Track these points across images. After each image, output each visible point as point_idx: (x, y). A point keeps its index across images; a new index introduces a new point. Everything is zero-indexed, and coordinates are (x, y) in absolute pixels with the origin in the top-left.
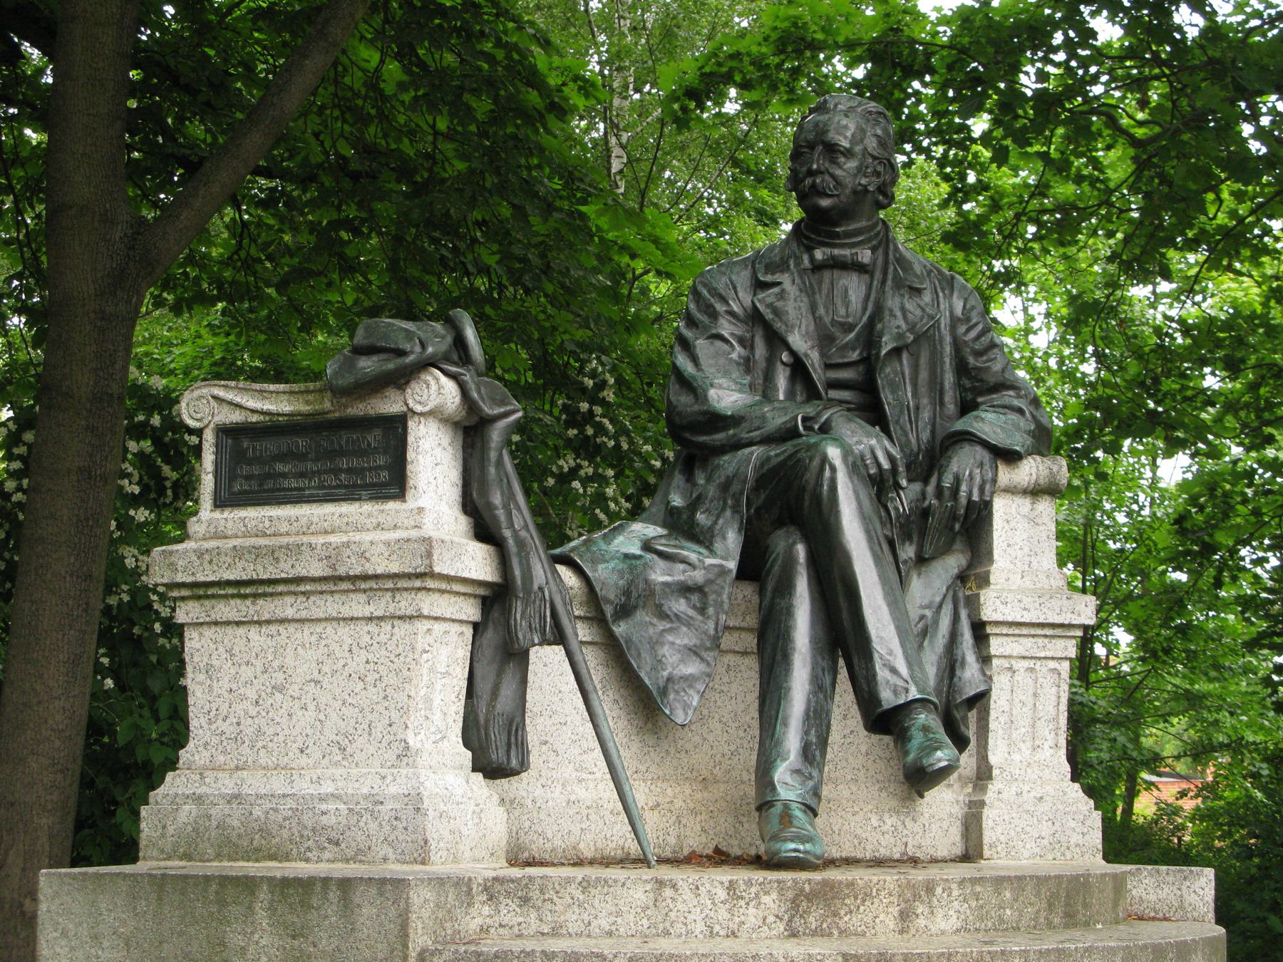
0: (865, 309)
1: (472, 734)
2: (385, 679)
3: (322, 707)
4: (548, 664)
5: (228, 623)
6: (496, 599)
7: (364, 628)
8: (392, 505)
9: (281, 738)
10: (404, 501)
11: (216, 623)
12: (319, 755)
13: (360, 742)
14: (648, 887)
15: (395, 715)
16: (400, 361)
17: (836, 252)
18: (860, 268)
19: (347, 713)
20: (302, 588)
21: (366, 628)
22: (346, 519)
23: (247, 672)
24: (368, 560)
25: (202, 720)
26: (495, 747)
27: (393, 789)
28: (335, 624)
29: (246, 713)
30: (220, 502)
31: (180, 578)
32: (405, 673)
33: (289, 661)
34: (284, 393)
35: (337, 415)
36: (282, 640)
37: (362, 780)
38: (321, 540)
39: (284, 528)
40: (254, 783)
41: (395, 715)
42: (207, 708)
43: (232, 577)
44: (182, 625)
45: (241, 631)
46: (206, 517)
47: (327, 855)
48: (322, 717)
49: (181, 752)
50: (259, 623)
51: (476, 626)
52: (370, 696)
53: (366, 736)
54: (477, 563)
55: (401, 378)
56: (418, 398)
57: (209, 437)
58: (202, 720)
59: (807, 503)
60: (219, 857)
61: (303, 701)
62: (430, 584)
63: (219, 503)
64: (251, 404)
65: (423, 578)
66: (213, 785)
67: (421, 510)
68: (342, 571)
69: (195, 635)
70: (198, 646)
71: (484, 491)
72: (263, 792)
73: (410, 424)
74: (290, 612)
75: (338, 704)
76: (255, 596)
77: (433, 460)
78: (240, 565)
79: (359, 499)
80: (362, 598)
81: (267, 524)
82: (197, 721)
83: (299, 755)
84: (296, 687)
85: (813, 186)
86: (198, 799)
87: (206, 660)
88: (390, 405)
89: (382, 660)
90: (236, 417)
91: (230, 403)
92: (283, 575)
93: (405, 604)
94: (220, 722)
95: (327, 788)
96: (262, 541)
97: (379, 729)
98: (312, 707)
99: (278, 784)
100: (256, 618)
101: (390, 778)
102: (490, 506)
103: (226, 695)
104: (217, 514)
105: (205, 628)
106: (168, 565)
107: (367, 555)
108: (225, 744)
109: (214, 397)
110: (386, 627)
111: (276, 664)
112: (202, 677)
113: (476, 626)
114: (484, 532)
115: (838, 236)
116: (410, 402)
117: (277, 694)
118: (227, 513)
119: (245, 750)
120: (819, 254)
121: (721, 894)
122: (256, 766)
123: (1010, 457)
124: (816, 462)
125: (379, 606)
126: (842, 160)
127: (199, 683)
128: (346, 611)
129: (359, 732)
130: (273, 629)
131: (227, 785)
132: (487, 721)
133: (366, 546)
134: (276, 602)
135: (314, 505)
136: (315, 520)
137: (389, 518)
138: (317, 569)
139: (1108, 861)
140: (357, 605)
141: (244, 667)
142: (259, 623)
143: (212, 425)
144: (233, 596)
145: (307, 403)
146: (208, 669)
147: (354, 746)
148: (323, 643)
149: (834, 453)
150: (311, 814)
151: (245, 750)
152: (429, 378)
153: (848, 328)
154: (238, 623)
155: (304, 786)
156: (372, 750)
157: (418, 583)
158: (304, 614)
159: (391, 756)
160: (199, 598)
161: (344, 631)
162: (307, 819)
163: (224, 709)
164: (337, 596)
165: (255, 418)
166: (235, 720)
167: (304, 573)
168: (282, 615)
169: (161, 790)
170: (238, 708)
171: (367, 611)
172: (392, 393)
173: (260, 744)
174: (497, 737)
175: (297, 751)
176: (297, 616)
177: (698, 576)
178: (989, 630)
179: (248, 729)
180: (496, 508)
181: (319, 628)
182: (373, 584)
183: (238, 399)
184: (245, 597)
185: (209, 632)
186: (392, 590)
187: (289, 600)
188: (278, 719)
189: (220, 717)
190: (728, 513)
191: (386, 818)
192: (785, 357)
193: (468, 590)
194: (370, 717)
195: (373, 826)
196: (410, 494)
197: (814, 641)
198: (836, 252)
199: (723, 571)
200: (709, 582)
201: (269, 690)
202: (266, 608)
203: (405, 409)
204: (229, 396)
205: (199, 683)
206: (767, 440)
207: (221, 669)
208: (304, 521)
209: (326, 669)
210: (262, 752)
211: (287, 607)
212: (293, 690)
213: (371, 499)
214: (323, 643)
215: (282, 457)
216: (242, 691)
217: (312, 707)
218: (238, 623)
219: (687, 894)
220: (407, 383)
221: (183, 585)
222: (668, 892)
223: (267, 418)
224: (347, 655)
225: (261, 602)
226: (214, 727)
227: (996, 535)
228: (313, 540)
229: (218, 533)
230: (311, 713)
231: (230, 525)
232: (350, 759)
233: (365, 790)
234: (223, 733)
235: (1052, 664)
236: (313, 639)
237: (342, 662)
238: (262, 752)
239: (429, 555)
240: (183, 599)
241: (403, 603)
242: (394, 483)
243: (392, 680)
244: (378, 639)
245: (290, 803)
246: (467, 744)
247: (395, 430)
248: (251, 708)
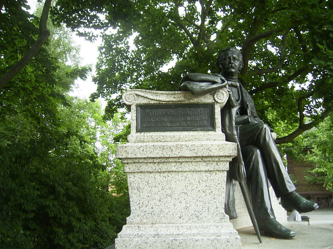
0: (239, 96)
2: (214, 192)
3: (188, 202)
7: (204, 174)
9: (171, 213)
10: (215, 131)
12: (188, 219)
13: (204, 214)
17: (233, 83)
18: (236, 87)
19: (198, 204)
20: (180, 160)
21: (205, 175)
22: (194, 137)
23: (155, 190)
24: (211, 151)
25: (136, 207)
28: (192, 173)
29: (155, 204)
30: (137, 131)
31: (129, 156)
33: (173, 185)
34: (165, 94)
35: (187, 102)
37: (209, 227)
39: (169, 139)
42: (138, 202)
45: (152, 175)
48: (188, 205)
49: (127, 218)
52: (208, 198)
53: (207, 211)
55: (212, 92)
56: (219, 98)
57: (133, 108)
58: (136, 207)
61: (180, 200)
63: (137, 131)
64: (151, 97)
66: (144, 230)
69: (132, 176)
70: (134, 180)
72: (168, 233)
73: (215, 106)
74: (174, 169)
78: (156, 152)
79: (197, 130)
80: (204, 164)
81: (162, 138)
83: (179, 219)
84: (176, 195)
85: (232, 66)
87: (137, 185)
89: (212, 185)
90: (145, 101)
91: (143, 97)
92: (175, 156)
94: (144, 207)
95: (195, 231)
97: (212, 209)
100: (159, 171)
101: (220, 227)
103: (147, 198)
104: (139, 134)
105: (136, 174)
107: (210, 149)
108: (146, 215)
109: (137, 95)
111: (167, 187)
112: (136, 191)
115: (233, 79)
116: (216, 99)
117: (169, 198)
118: (142, 134)
126: (236, 61)
127: (134, 193)
128: (198, 169)
129: (204, 211)
130: (166, 174)
134: (168, 165)
136: (182, 137)
137: (212, 137)
141: (154, 188)
142: (160, 172)
143: (135, 104)
145: (174, 98)
147: (202, 215)
148: (188, 179)
150: (191, 241)
151: (155, 217)
156: (210, 217)
158: (180, 169)
161: (196, 175)
163: (146, 203)
164: (193, 163)
165: (153, 102)
166: (151, 207)
168: (171, 170)
169: (120, 233)
170: (152, 203)
172: (208, 96)
173: (162, 215)
175: (178, 218)
176: (177, 170)
179: (157, 210)
181: (185, 174)
182: (210, 159)
183: (146, 95)
185: (137, 175)
186: (217, 161)
187: (173, 164)
188: (169, 206)
189: (144, 206)
191: (224, 242)
194: (208, 205)
198: (233, 83)
201: (165, 196)
202: (164, 167)
203: (213, 101)
205: (134, 193)
208: (177, 137)
209: (189, 188)
210: (163, 218)
213: (201, 130)
214: (188, 179)
216: (153, 196)
217: (184, 202)
223: (158, 102)
224: (198, 184)
225: (161, 165)
226: (141, 209)
228: (187, 143)
231: (146, 138)
232: (201, 220)
234: (145, 211)
236: (183, 178)
237: (196, 186)
238: (163, 218)
241: (221, 166)
244: (210, 178)
248: (157, 202)
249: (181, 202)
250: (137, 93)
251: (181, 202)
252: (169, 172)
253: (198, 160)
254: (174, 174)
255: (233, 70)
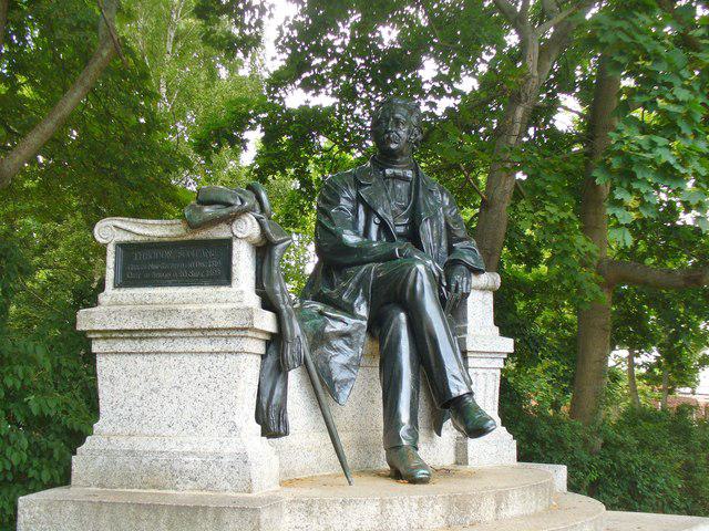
1: (261, 416)
4: (294, 377)
5: (124, 353)
6: (276, 341)
7: (207, 358)
8: (223, 289)
11: (116, 353)
14: (378, 504)
15: (227, 408)
16: (230, 209)
17: (396, 171)
18: (405, 179)
23: (135, 381)
26: (271, 421)
27: (228, 450)
30: (117, 286)
31: (96, 328)
32: (233, 384)
33: (161, 375)
36: (157, 363)
38: (183, 308)
39: (158, 300)
40: (141, 444)
41: (227, 408)
43: (128, 328)
44: (95, 354)
45: (131, 358)
46: (110, 294)
47: (189, 487)
50: (143, 353)
51: (262, 356)
54: (267, 322)
55: (229, 220)
57: (111, 250)
59: (407, 294)
60: (122, 486)
62: (250, 334)
63: (117, 286)
64: (137, 230)
65: (243, 331)
67: (242, 292)
68: (197, 325)
71: (270, 283)
74: (162, 348)
75: (192, 400)
76: (173, 338)
77: (243, 263)
82: (104, 407)
85: (389, 138)
86: (107, 452)
88: (221, 232)
90: (128, 238)
92: (161, 327)
93: (233, 345)
95: (187, 448)
96: (147, 307)
98: (176, 401)
99: (156, 445)
102: (274, 292)
104: (116, 291)
106: (87, 320)
110: (222, 357)
113: (262, 356)
114: (268, 303)
115: (397, 163)
118: (122, 290)
119: (135, 425)
120: (388, 171)
121: (415, 506)
122: (141, 434)
123: (477, 272)
124: (413, 273)
125: (219, 346)
130: (151, 357)
131: (125, 444)
132: (268, 408)
133: (212, 312)
135: (176, 288)
138: (181, 324)
139: (518, 460)
140: (204, 345)
142: (143, 353)
144: (127, 338)
146: (111, 379)
149: (421, 267)
151: (135, 425)
152: (247, 219)
153: (404, 209)
154: (129, 354)
155: (172, 446)
157: (243, 333)
158: (171, 349)
159: (225, 430)
160: (106, 338)
161: (196, 360)
162: (177, 466)
165: (139, 239)
167: (173, 326)
171: (210, 348)
172: (223, 226)
174: (273, 416)
177: (348, 328)
178: (469, 355)
179: (136, 413)
180: (277, 292)
181: (180, 357)
184: (135, 338)
186: (225, 337)
190: (360, 297)
192: (377, 220)
193: (261, 336)
195: (218, 471)
196: (234, 283)
197: (412, 361)
198: (396, 171)
199: (361, 327)
200: (356, 331)
202: (148, 345)
204: (124, 226)
206: (377, 260)
207: (116, 375)
209: (184, 380)
211: (161, 345)
212: (164, 392)
215: (154, 261)
217: (176, 401)
218: (129, 354)
219: (397, 506)
220: (233, 221)
221: (98, 331)
222: (388, 506)
225: (144, 342)
227: (469, 309)
229: (117, 306)
230: (175, 406)
233: (211, 450)
235: (494, 371)
239: (251, 318)
240: (96, 339)
242: (224, 276)
243: (224, 387)
245: (165, 456)
246: (258, 421)
247: (225, 246)
249: (171, 402)
250: (119, 224)
251: (171, 402)
252: (157, 353)
253: (197, 334)
254: (163, 357)
255: (393, 146)
